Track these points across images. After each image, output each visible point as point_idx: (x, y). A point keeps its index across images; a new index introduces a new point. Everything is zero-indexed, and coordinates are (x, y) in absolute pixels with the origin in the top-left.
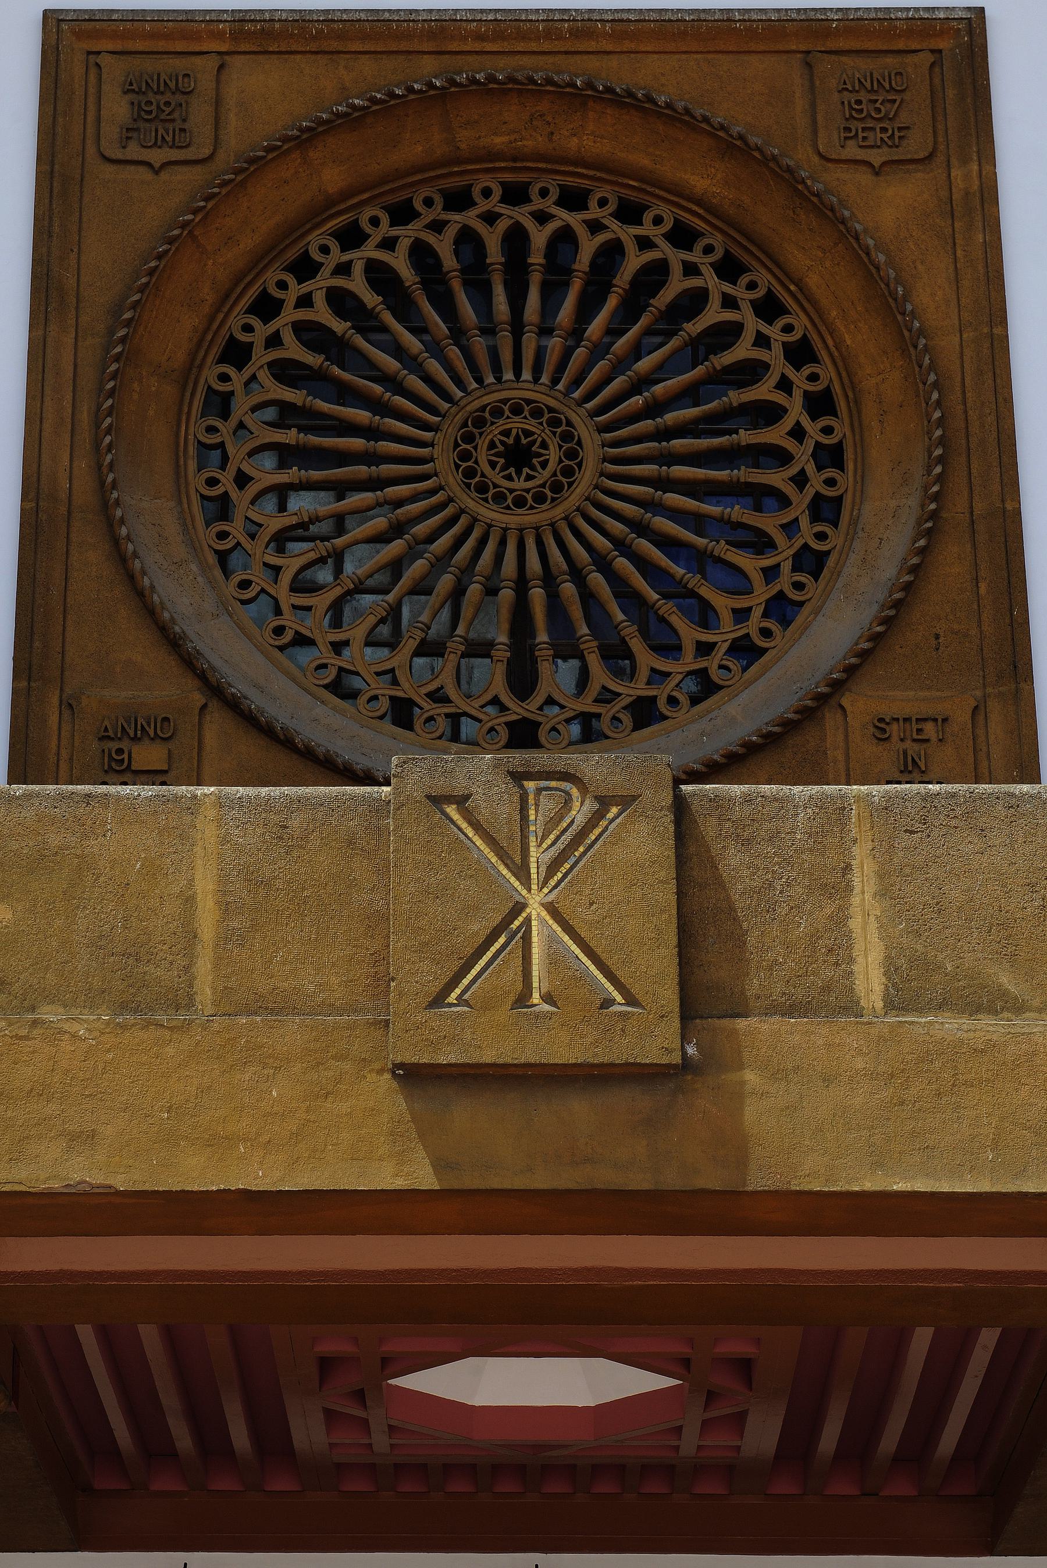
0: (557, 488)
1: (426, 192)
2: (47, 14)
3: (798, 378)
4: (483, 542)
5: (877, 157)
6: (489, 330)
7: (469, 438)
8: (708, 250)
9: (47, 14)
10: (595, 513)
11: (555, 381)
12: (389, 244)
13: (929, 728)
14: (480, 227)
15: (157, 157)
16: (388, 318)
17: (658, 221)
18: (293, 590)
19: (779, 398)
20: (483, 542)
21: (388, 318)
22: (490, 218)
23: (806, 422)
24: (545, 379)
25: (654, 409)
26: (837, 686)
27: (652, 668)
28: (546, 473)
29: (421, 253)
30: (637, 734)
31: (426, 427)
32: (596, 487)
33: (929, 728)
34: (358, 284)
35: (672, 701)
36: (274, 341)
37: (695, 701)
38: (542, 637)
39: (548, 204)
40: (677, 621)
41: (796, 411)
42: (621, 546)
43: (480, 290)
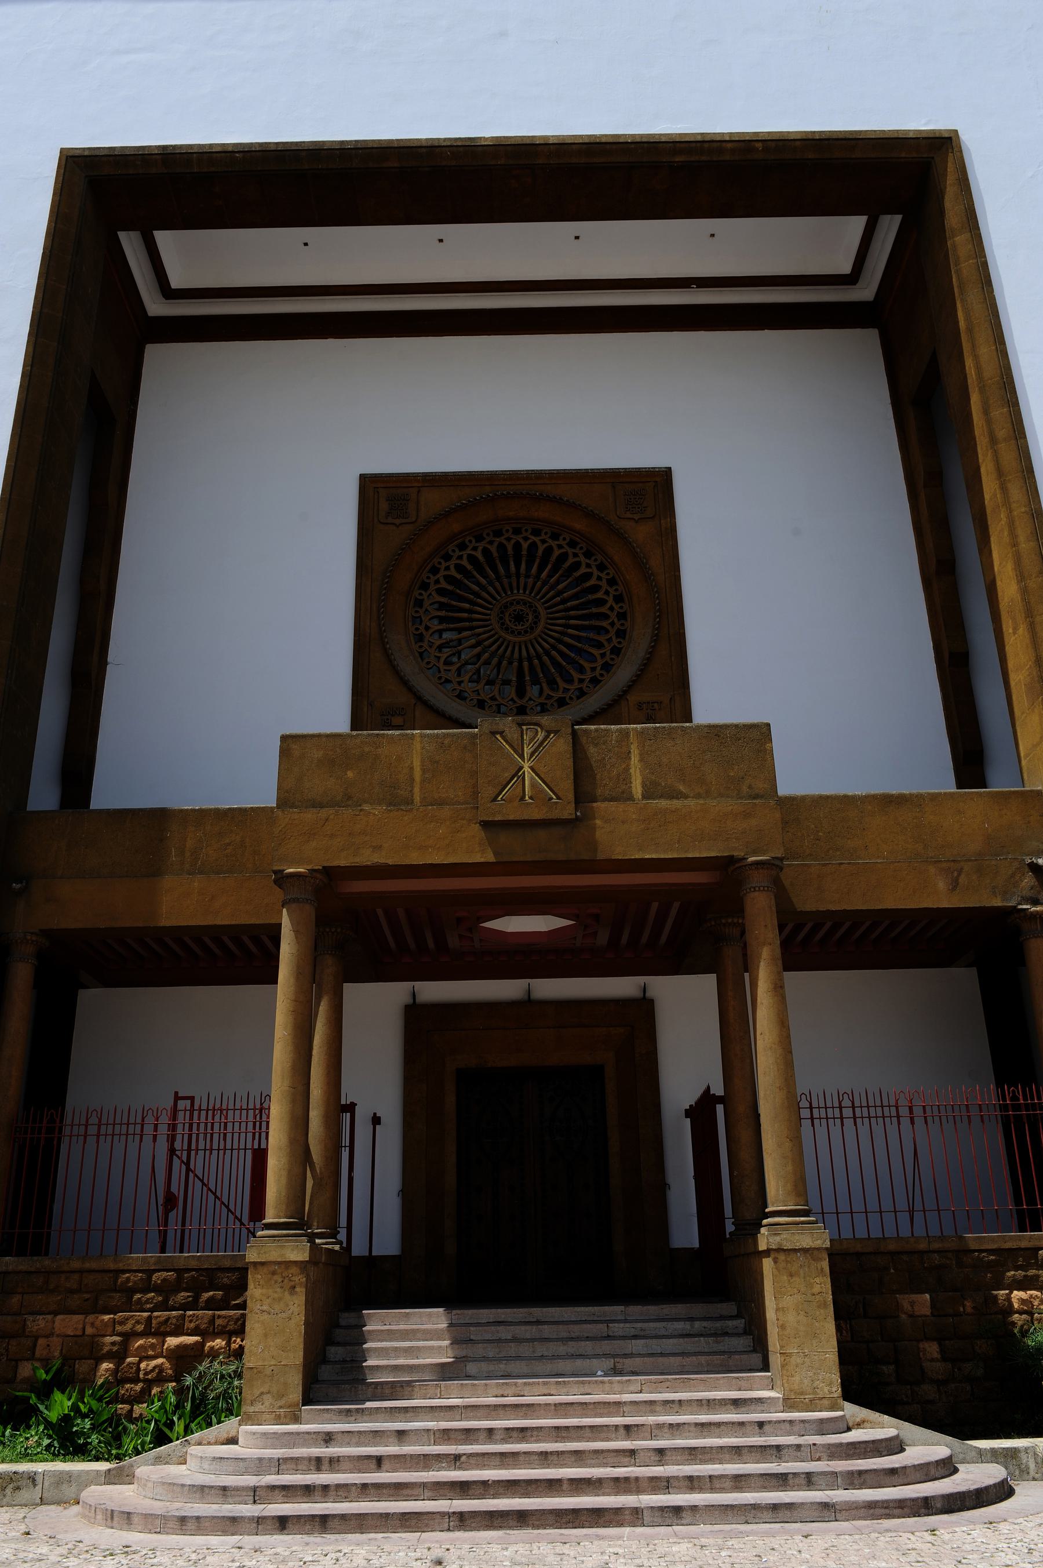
2: (363, 477)
3: (611, 591)
8: (581, 548)
11: (531, 593)
15: (398, 521)
24: (527, 592)
35: (571, 698)
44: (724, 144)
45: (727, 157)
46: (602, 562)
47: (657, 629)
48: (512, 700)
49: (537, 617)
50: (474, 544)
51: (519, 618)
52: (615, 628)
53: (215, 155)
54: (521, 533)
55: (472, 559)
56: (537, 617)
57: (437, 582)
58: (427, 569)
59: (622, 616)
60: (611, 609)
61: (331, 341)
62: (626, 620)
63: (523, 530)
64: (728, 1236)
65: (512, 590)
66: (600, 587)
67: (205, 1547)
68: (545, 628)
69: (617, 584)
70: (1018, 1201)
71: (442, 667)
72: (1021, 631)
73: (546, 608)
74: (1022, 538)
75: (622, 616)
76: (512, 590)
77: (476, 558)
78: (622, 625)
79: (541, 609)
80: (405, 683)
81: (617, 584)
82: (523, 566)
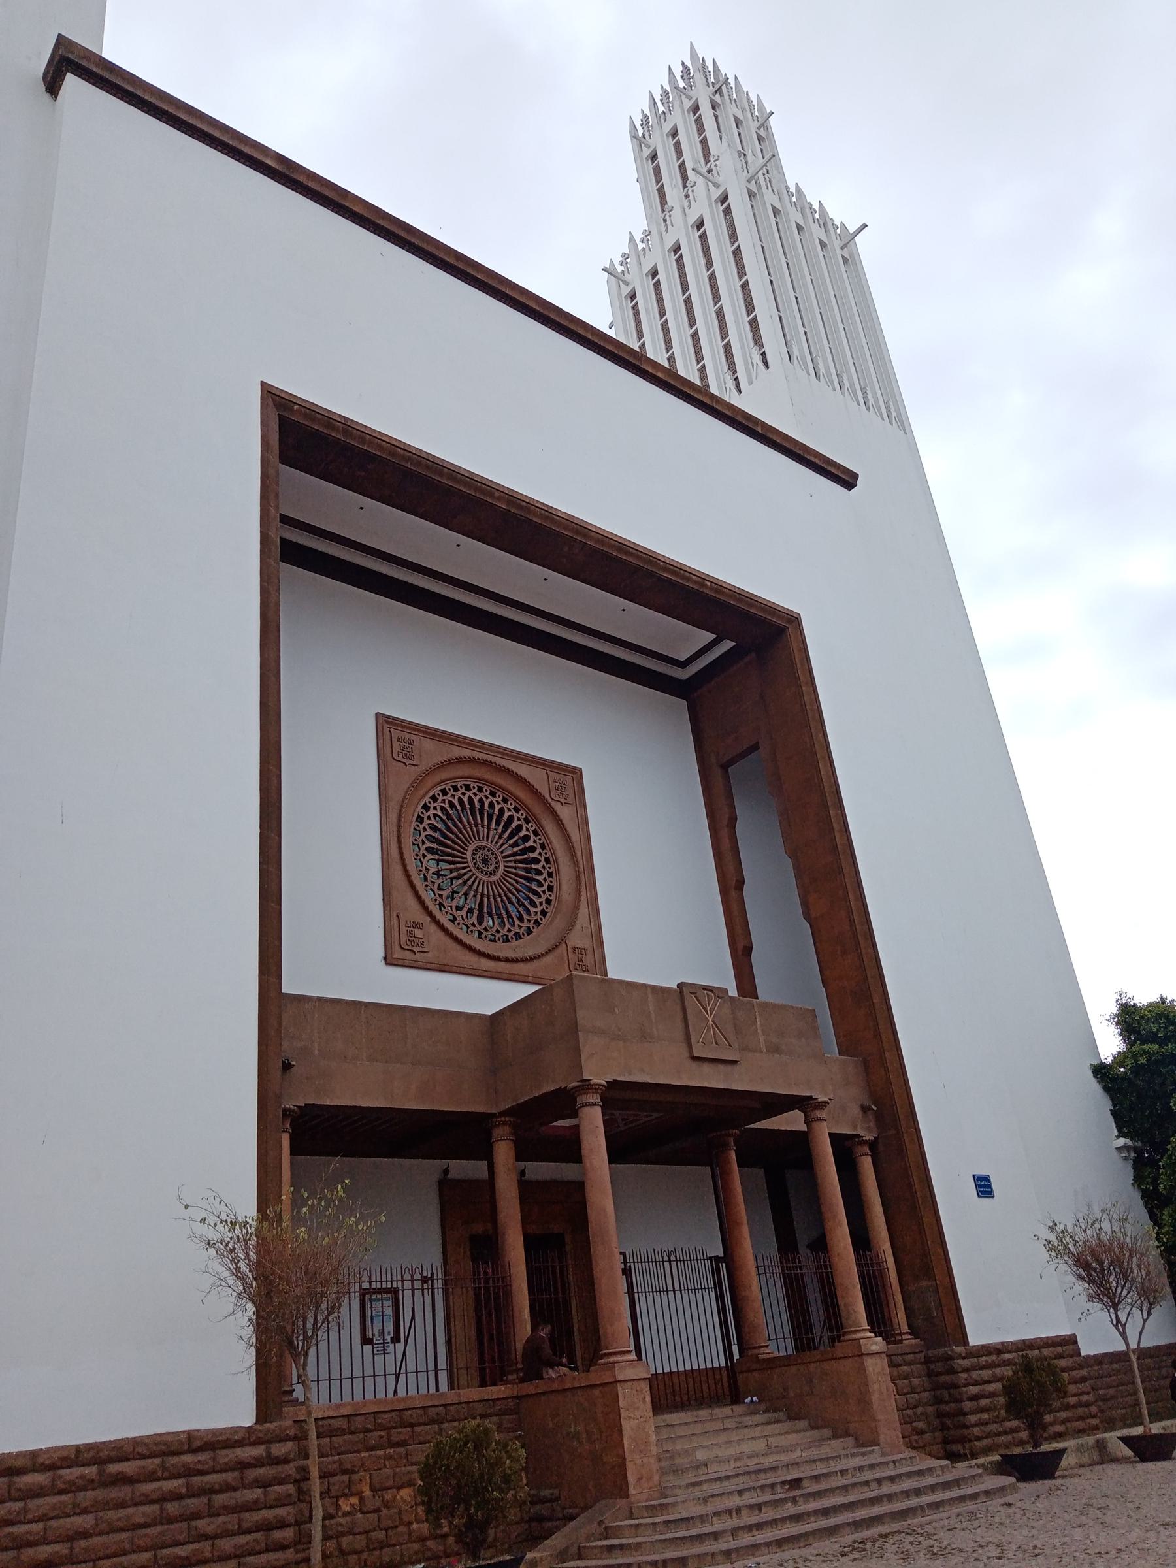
0: (486, 874)
3: (544, 905)
6: (483, 826)
7: (480, 848)
8: (550, 868)
10: (485, 885)
12: (509, 810)
14: (516, 819)
16: (503, 824)
17: (546, 853)
18: (425, 836)
19: (538, 904)
21: (503, 824)
25: (454, 856)
27: (1117, 1148)
32: (484, 881)
34: (507, 814)
35: (486, 937)
36: (464, 794)
37: (490, 941)
43: (498, 824)
46: (430, 798)
48: (451, 907)
49: (495, 871)
50: (511, 807)
51: (485, 861)
54: (543, 850)
55: (511, 818)
58: (479, 785)
63: (539, 837)
66: (540, 897)
67: (554, 884)
69: (544, 917)
70: (474, 1275)
71: (423, 837)
75: (537, 923)
77: (520, 831)
79: (471, 863)
81: (544, 917)
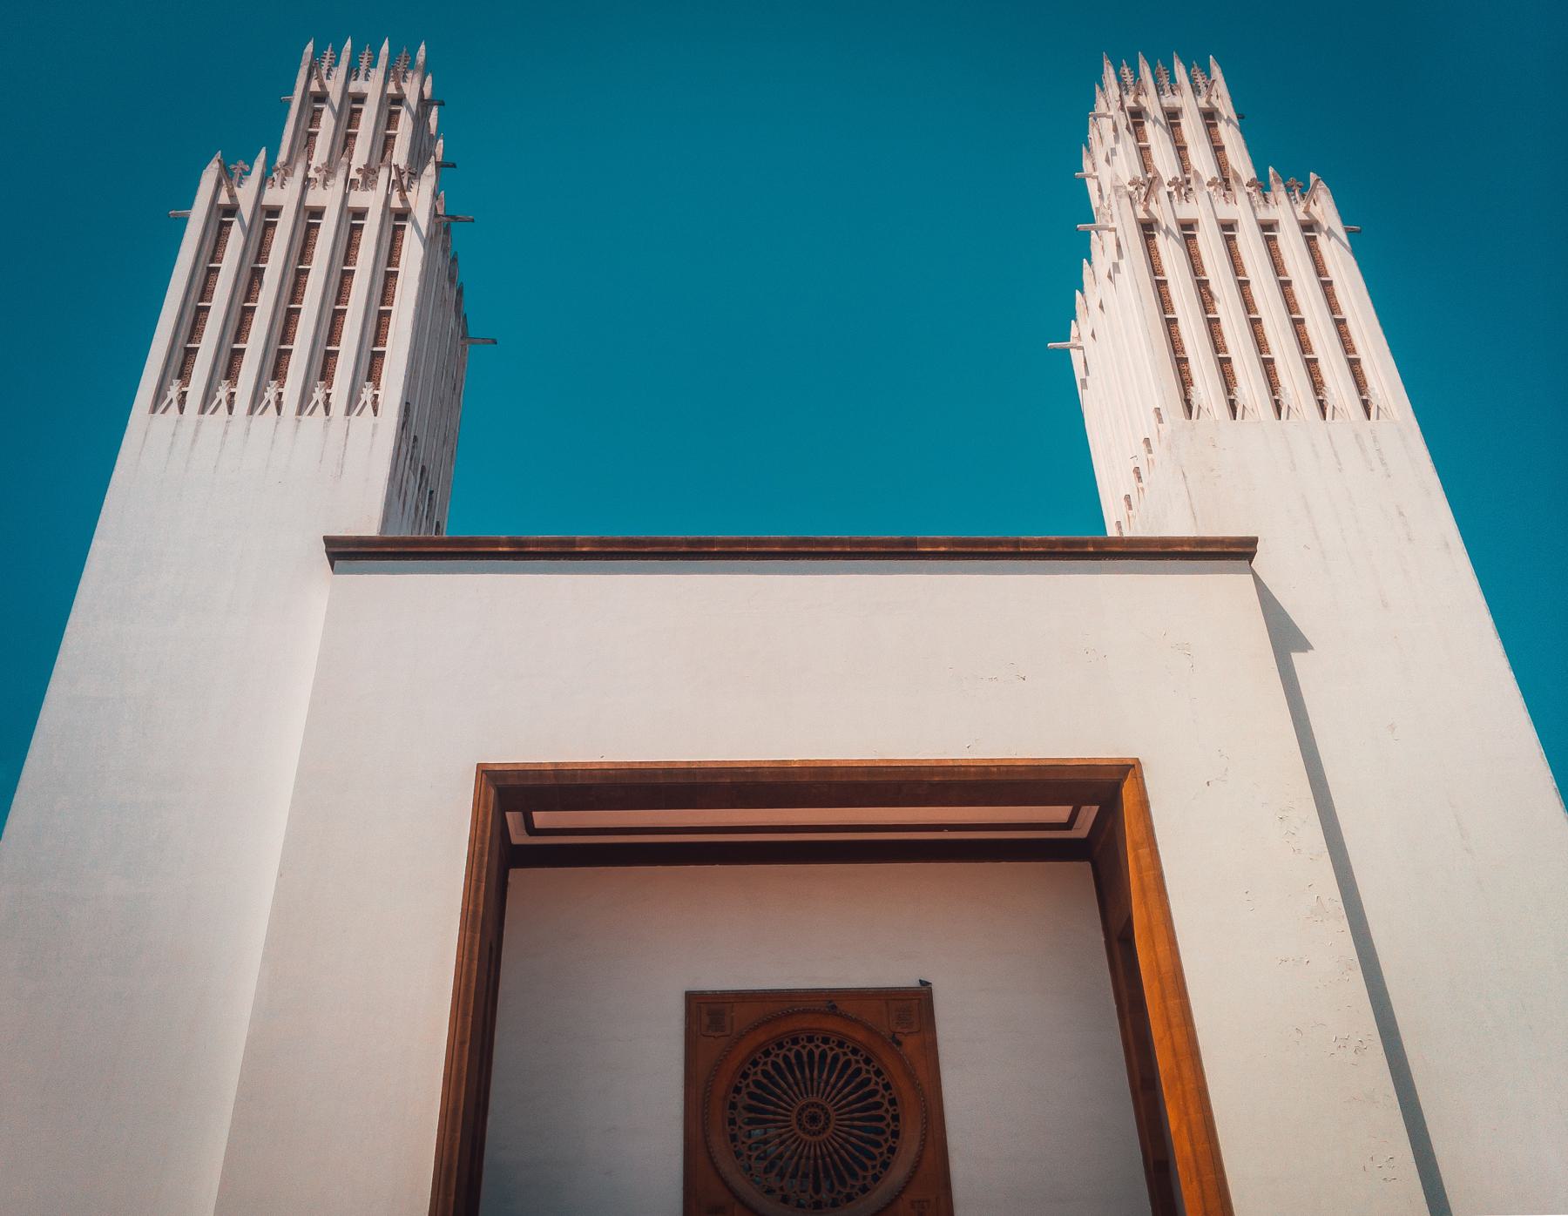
1: (787, 1039)
2: (687, 993)
4: (836, 1135)
5: (906, 1031)
7: (826, 1113)
9: (687, 993)
11: (822, 1096)
13: (925, 1204)
15: (717, 1034)
20: (836, 1135)
22: (883, 1096)
23: (761, 1064)
24: (824, 1098)
26: (901, 1192)
28: (809, 1127)
29: (786, 1058)
30: (849, 1204)
31: (788, 1111)
33: (925, 1204)
38: (822, 1175)
39: (819, 1043)
40: (872, 1149)
41: (811, 1046)
42: (836, 1151)
44: (969, 769)
45: (972, 778)
47: (924, 1134)
52: (861, 1061)
53: (611, 772)
56: (828, 1119)
57: (748, 1086)
59: (878, 1073)
60: (877, 1083)
61: (659, 868)
62: (883, 1074)
64: (1194, 63)
65: (807, 1094)
68: (835, 1129)
72: (1194, 1183)
73: (835, 1110)
74: (1192, 1111)
75: (878, 1073)
76: (807, 1094)
78: (896, 1126)
79: (831, 1111)
80: (725, 1183)
82: (816, 1072)
